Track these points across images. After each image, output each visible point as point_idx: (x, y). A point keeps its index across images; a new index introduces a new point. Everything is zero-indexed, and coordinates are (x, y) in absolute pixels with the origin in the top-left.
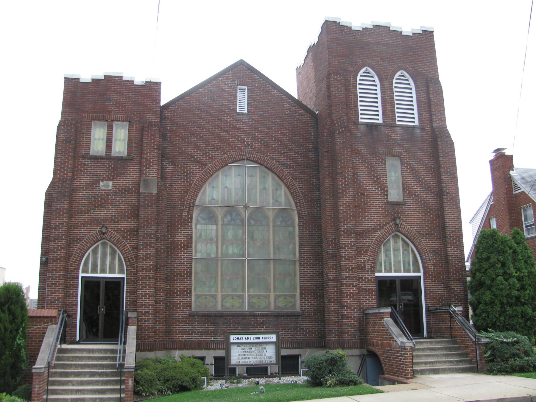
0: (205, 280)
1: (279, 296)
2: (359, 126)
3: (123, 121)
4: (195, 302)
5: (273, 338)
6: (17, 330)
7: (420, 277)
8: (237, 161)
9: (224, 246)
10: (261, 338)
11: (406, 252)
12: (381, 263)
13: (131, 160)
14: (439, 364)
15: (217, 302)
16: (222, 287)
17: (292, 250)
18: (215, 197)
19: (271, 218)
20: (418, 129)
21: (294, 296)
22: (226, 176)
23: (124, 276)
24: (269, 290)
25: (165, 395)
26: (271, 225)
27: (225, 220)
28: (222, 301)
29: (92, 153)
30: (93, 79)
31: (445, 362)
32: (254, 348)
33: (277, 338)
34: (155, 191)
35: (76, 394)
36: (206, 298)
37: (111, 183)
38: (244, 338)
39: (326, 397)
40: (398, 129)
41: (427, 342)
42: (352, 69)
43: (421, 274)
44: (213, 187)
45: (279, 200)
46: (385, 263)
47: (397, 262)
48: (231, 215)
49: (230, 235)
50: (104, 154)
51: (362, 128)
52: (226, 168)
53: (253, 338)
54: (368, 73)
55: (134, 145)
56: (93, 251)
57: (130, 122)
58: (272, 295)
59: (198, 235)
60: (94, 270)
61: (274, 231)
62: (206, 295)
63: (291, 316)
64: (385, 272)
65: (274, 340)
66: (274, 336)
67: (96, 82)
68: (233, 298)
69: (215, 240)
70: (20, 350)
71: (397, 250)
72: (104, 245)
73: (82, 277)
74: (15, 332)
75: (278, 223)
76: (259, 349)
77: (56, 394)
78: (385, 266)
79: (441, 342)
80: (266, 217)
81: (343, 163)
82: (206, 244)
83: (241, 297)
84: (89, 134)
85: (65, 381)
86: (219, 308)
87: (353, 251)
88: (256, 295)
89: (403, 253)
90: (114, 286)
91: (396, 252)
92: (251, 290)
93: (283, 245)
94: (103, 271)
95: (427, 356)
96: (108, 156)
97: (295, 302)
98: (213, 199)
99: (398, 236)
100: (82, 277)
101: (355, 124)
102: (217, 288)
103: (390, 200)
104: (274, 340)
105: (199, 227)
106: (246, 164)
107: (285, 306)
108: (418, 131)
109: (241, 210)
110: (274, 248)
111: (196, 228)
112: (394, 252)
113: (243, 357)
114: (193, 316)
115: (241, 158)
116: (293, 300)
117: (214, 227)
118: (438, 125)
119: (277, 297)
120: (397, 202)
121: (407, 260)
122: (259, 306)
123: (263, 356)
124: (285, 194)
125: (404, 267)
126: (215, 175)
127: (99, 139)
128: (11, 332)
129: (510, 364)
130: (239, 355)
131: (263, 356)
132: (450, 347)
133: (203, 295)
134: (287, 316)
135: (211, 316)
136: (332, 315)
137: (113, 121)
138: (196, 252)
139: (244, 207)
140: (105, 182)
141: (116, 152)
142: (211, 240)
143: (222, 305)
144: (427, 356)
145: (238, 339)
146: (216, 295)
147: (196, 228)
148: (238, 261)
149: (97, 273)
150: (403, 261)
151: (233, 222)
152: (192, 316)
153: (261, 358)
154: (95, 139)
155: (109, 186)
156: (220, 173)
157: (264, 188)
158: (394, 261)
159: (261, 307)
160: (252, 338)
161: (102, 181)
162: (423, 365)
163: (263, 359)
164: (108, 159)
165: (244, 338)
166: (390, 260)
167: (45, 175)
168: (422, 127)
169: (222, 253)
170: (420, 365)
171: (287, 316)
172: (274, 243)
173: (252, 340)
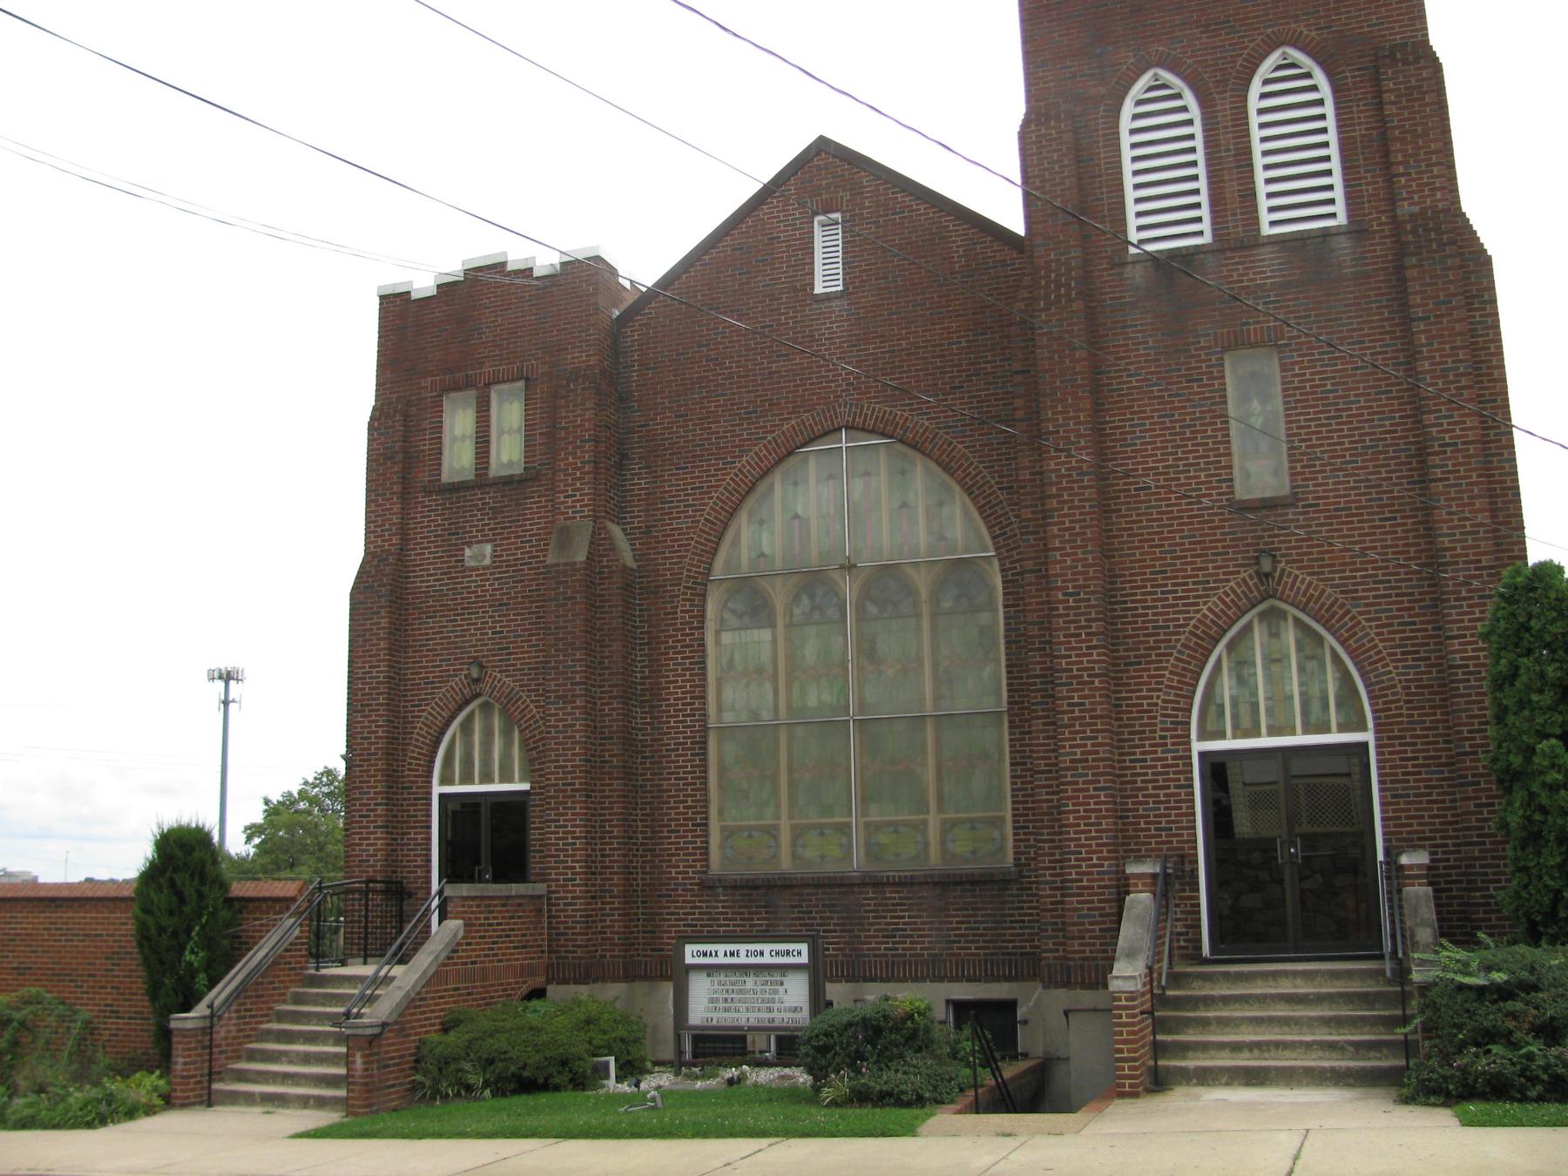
0: (745, 786)
1: (955, 823)
2: (1129, 268)
3: (513, 380)
4: (722, 846)
5: (801, 953)
6: (188, 931)
7: (1365, 745)
8: (821, 436)
9: (796, 685)
10: (767, 953)
11: (1311, 665)
12: (1222, 706)
13: (533, 479)
14: (1287, 1053)
15: (778, 846)
16: (792, 802)
17: (983, 685)
18: (766, 550)
19: (924, 593)
20: (1343, 238)
21: (997, 822)
22: (796, 484)
23: (1368, 736)
24: (923, 806)
25: (476, 1099)
26: (925, 610)
27: (797, 611)
28: (793, 844)
29: (446, 476)
30: (439, 286)
31: (1308, 1046)
32: (750, 982)
33: (813, 953)
34: (581, 557)
35: (282, 1083)
36: (750, 836)
37: (488, 548)
38: (720, 953)
39: (394, 1136)
40: (1266, 253)
41: (1295, 974)
42: (1103, 90)
43: (1368, 736)
44: (762, 522)
45: (948, 535)
46: (1234, 704)
47: (1280, 701)
48: (812, 597)
49: (810, 652)
50: (469, 475)
51: (1137, 275)
52: (792, 460)
53: (744, 953)
54: (1293, 65)
55: (539, 440)
56: (1231, 647)
57: (527, 379)
58: (933, 820)
59: (725, 660)
60: (467, 778)
61: (934, 628)
62: (749, 828)
63: (985, 882)
64: (1234, 737)
65: (804, 959)
66: (804, 947)
67: (447, 290)
68: (822, 834)
69: (770, 670)
70: (193, 977)
71: (1279, 661)
72: (486, 708)
73: (442, 796)
74: (182, 937)
75: (947, 604)
76: (766, 983)
77: (247, 1080)
78: (1235, 716)
79: (1349, 974)
80: (910, 591)
81: (1061, 400)
82: (748, 685)
83: (844, 829)
84: (439, 428)
85: (274, 1052)
86: (786, 864)
87: (1097, 676)
88: (889, 824)
89: (1301, 669)
90: (509, 810)
91: (1275, 668)
92: (874, 809)
93: (952, 672)
94: (487, 778)
95: (1258, 1021)
96: (482, 480)
97: (1003, 838)
98: (762, 555)
99: (1283, 615)
100: (442, 796)
101: (1114, 266)
102: (778, 807)
103: (1241, 493)
104: (804, 959)
105: (726, 637)
106: (844, 441)
107: (974, 852)
108: (1343, 243)
109: (836, 576)
110: (936, 679)
111: (718, 642)
112: (1264, 668)
113: (721, 1005)
114: (711, 888)
115: (827, 425)
116: (996, 834)
117: (765, 635)
118: (1417, 209)
119: (947, 827)
120: (1271, 499)
121: (1315, 690)
122: (897, 855)
123: (776, 1006)
124: (966, 514)
125: (1305, 713)
126: (762, 487)
127: (463, 438)
128: (175, 934)
129: (1459, 1068)
130: (712, 1000)
131: (776, 1006)
132: (1366, 994)
133: (741, 829)
134: (973, 883)
135: (757, 888)
136: (1047, 882)
137: (488, 385)
138: (720, 709)
139: (842, 567)
140: (476, 548)
141: (502, 466)
142: (760, 671)
143: (794, 856)
144: (1258, 1021)
145: (705, 954)
146: (776, 827)
147: (718, 642)
148: (831, 728)
149: (472, 782)
150: (1302, 694)
151: (816, 616)
152: (708, 886)
153: (770, 1010)
154: (454, 439)
155: (484, 556)
156: (777, 478)
157: (904, 505)
158: (1267, 699)
159: (903, 857)
160: (743, 953)
161: (469, 544)
162: (1225, 1053)
163: (775, 1015)
164: (481, 487)
165: (721, 954)
166: (1255, 694)
167: (347, 549)
168: (1357, 228)
169: (789, 707)
170: (1212, 1053)
171: (816, 886)
172: (935, 666)
173: (742, 960)
